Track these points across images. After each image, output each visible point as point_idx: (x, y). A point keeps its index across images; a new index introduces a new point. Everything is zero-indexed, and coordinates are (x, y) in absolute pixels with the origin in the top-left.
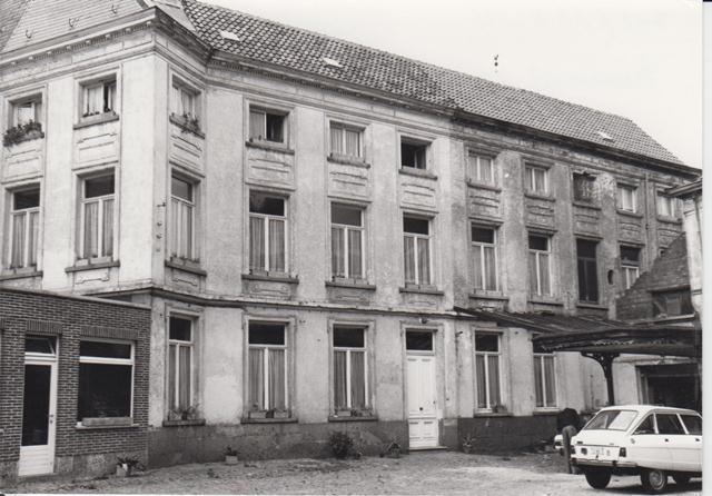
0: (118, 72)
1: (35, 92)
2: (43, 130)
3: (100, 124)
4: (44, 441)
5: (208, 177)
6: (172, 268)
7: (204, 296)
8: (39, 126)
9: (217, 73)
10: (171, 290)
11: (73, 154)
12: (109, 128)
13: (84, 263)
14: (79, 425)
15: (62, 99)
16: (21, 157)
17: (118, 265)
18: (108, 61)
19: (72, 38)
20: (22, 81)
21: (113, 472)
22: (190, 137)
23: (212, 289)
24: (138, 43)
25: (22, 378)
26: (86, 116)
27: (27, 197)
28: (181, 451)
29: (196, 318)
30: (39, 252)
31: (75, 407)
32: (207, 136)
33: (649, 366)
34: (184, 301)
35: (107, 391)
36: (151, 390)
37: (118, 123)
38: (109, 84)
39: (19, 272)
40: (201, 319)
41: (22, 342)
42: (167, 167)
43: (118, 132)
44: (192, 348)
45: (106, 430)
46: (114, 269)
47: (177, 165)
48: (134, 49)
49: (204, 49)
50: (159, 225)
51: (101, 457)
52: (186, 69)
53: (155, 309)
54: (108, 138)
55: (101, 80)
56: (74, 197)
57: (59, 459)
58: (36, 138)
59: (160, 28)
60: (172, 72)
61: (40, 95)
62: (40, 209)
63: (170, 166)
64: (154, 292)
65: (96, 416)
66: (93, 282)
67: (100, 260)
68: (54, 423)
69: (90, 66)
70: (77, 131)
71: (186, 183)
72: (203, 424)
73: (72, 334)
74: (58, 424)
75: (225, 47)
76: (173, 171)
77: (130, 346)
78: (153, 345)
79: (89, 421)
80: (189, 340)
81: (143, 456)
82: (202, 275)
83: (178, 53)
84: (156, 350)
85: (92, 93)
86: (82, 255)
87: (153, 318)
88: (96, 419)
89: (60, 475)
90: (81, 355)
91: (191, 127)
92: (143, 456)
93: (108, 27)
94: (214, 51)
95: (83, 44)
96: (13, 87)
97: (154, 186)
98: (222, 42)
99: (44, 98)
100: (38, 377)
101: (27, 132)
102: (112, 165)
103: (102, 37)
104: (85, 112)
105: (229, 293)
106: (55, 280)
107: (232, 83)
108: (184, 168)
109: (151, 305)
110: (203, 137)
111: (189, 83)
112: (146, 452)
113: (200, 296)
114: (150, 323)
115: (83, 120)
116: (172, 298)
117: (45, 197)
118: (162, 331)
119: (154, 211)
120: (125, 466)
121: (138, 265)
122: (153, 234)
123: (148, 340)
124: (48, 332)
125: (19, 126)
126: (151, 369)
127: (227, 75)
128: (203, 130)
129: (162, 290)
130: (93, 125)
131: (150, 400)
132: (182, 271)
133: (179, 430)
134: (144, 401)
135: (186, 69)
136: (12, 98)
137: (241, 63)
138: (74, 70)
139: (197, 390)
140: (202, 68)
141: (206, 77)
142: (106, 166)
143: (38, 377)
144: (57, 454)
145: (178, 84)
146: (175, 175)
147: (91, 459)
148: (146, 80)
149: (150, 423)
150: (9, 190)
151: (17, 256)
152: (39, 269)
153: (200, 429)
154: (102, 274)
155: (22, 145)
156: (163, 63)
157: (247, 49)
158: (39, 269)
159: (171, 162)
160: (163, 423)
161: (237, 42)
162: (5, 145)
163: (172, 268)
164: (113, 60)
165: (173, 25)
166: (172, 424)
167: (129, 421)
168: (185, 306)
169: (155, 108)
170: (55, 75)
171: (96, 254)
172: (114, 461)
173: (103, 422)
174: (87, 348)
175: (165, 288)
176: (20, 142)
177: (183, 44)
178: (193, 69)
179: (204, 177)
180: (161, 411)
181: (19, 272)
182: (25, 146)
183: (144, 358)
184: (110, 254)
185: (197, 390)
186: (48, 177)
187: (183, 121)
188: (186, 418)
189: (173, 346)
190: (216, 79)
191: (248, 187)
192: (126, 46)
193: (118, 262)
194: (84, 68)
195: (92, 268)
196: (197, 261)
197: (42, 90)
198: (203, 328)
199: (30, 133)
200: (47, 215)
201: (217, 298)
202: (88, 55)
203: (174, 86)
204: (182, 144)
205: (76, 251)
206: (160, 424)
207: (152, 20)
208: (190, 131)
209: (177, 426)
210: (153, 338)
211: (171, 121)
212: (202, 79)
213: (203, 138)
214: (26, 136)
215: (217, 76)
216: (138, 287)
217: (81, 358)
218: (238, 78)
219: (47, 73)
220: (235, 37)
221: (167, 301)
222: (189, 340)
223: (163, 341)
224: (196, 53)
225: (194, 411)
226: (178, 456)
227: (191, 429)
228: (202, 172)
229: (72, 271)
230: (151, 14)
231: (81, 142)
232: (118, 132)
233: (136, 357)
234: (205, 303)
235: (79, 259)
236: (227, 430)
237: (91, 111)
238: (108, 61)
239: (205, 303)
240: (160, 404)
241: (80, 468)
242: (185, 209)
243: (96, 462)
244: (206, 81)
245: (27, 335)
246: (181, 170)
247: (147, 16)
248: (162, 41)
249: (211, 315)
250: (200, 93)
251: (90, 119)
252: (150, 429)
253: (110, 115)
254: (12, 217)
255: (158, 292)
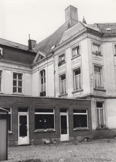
0: (80, 44)
1: (63, 53)
2: (65, 61)
3: (77, 57)
4: (66, 133)
5: (104, 66)
6: (96, 90)
7: (106, 96)
8: (65, 60)
9: (105, 39)
10: (96, 95)
11: (71, 65)
12: (78, 58)
13: (75, 91)
14: (74, 129)
15: (69, 53)
16: (62, 68)
17: (83, 90)
18: (77, 43)
19: (70, 39)
20: (61, 51)
21: (84, 141)
22: (98, 56)
23: (107, 94)
24: (84, 36)
25: (73, 117)
26: (73, 56)
27: (63, 77)
28: (102, 135)
29: (104, 102)
30: (66, 89)
31: (73, 125)
32: (103, 56)
33: (75, 109)
34: (100, 98)
35: (81, 121)
36: (92, 120)
37: (80, 57)
38: (78, 48)
39: (63, 94)
40: (105, 102)
41: (59, 110)
42: (92, 65)
43: (80, 59)
44: (103, 109)
45: (81, 130)
46: (82, 92)
47: (95, 64)
48: (83, 38)
49: (100, 34)
50: (91, 79)
51: (81, 137)
52: (96, 40)
53: (92, 100)
54: (78, 61)
55: (76, 47)
56: (72, 76)
57: (70, 137)
58: (64, 64)
59: (88, 32)
60: (92, 42)
61: (64, 54)
62: (66, 79)
63: (93, 65)
64: (91, 96)
65: (79, 127)
66: (78, 95)
67: (79, 89)
68: (68, 129)
69: (74, 45)
70: (72, 60)
71: (98, 68)
72: (108, 129)
73: (71, 108)
74: (69, 129)
75: (107, 32)
76: (94, 66)
77: (53, 109)
78: (92, 109)
79: (76, 128)
80: (102, 108)
81: (91, 137)
82: (105, 91)
83: (94, 37)
84: (93, 110)
85: (75, 51)
86: (75, 89)
87: (91, 103)
88: (78, 128)
89: (71, 141)
90: (36, 112)
91: (99, 54)
92: (91, 137)
93: (76, 35)
94: (103, 34)
95: (72, 40)
96: (59, 53)
97: (89, 70)
98: (106, 31)
99: (65, 54)
100: (64, 118)
101: (62, 62)
102: (79, 67)
103: (76, 37)
104: (74, 55)
105: (113, 95)
106: (70, 96)
107: (109, 41)
108: (97, 65)
109: (91, 100)
110: (102, 56)
111: (97, 43)
112: (92, 136)
113: (104, 96)
114: (91, 104)
115: (73, 57)
116: (96, 97)
117: (67, 77)
118: (94, 106)
119: (90, 76)
120: (86, 139)
121: (87, 90)
122: (90, 82)
123: (91, 108)
124: (65, 107)
125: (61, 61)
126: (92, 115)
127: (108, 39)
128: (102, 54)
129: (93, 95)
130: (75, 58)
131: (92, 123)
132: (98, 90)
133: (101, 130)
134: (91, 123)
135: (96, 40)
136: (59, 55)
137: (111, 35)
138: (70, 46)
139: (105, 120)
140: (101, 39)
141: (102, 41)
142: (79, 67)
143: (64, 118)
144: (70, 136)
145: (94, 44)
146: (95, 66)
147: (78, 137)
148: (86, 44)
149: (93, 129)
150: (60, 76)
151: (63, 91)
152: (67, 93)
153: (107, 130)
154: (79, 93)
155: (61, 66)
156: (90, 40)
157: (114, 31)
158: (67, 93)
159: (93, 64)
160: (96, 128)
161: (111, 30)
162: (58, 66)
163: (96, 90)
164: (78, 42)
165: (92, 30)
166: (98, 129)
167: (88, 128)
168: (100, 99)
169: (88, 51)
170: (67, 48)
171: (78, 89)
172: (84, 138)
173: (78, 129)
174: (75, 111)
175: (94, 95)
176: (61, 65)
177: (95, 34)
178: (98, 40)
179: (103, 66)
180: (96, 125)
181: (63, 94)
182: (62, 66)
183: (90, 113)
184: (81, 88)
185: (105, 120)
186: (67, 72)
187: (96, 53)
188: (102, 128)
189: (98, 109)
190: (104, 41)
191: (93, 65)
192: (81, 38)
193: (83, 90)
194: (73, 45)
195: (77, 92)
196: (103, 88)
197: (65, 52)
198: (106, 104)
199: (63, 63)
200: (67, 80)
201: (109, 96)
202: (73, 42)
203: (93, 45)
204: (96, 58)
205: (74, 88)
206: (95, 129)
207: (86, 30)
208: (98, 55)
209: (100, 129)
210: (92, 108)
211: (93, 53)
212: (101, 41)
213: (102, 56)
214: (62, 63)
215: (105, 40)
216: (87, 95)
217: (74, 113)
218: (111, 39)
219: (66, 48)
220: (110, 29)
221: (95, 98)
222: (102, 108)
223: (95, 108)
224: (99, 36)
225: (105, 125)
226: (101, 137)
227: (104, 130)
228: (103, 65)
229: (73, 93)
230: (86, 29)
231: (73, 62)
232: (80, 59)
233: (88, 113)
234: (106, 98)
235: (75, 90)
236: (114, 130)
237: (75, 55)
238: (77, 43)
239: (106, 98)
240: (95, 124)
241: (75, 139)
242: (99, 75)
243: (79, 138)
244: (102, 42)
245: (18, 108)
246: (97, 65)
247: (85, 30)
248: (89, 35)
249: (108, 101)
250: (100, 45)
251: (74, 57)
252: (93, 130)
253: (79, 55)
254: (61, 82)
255: (92, 96)
